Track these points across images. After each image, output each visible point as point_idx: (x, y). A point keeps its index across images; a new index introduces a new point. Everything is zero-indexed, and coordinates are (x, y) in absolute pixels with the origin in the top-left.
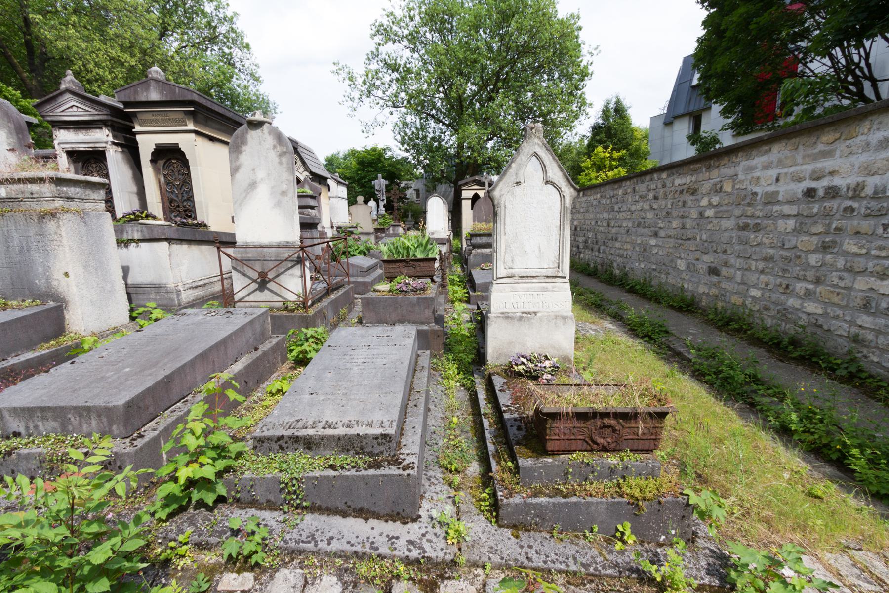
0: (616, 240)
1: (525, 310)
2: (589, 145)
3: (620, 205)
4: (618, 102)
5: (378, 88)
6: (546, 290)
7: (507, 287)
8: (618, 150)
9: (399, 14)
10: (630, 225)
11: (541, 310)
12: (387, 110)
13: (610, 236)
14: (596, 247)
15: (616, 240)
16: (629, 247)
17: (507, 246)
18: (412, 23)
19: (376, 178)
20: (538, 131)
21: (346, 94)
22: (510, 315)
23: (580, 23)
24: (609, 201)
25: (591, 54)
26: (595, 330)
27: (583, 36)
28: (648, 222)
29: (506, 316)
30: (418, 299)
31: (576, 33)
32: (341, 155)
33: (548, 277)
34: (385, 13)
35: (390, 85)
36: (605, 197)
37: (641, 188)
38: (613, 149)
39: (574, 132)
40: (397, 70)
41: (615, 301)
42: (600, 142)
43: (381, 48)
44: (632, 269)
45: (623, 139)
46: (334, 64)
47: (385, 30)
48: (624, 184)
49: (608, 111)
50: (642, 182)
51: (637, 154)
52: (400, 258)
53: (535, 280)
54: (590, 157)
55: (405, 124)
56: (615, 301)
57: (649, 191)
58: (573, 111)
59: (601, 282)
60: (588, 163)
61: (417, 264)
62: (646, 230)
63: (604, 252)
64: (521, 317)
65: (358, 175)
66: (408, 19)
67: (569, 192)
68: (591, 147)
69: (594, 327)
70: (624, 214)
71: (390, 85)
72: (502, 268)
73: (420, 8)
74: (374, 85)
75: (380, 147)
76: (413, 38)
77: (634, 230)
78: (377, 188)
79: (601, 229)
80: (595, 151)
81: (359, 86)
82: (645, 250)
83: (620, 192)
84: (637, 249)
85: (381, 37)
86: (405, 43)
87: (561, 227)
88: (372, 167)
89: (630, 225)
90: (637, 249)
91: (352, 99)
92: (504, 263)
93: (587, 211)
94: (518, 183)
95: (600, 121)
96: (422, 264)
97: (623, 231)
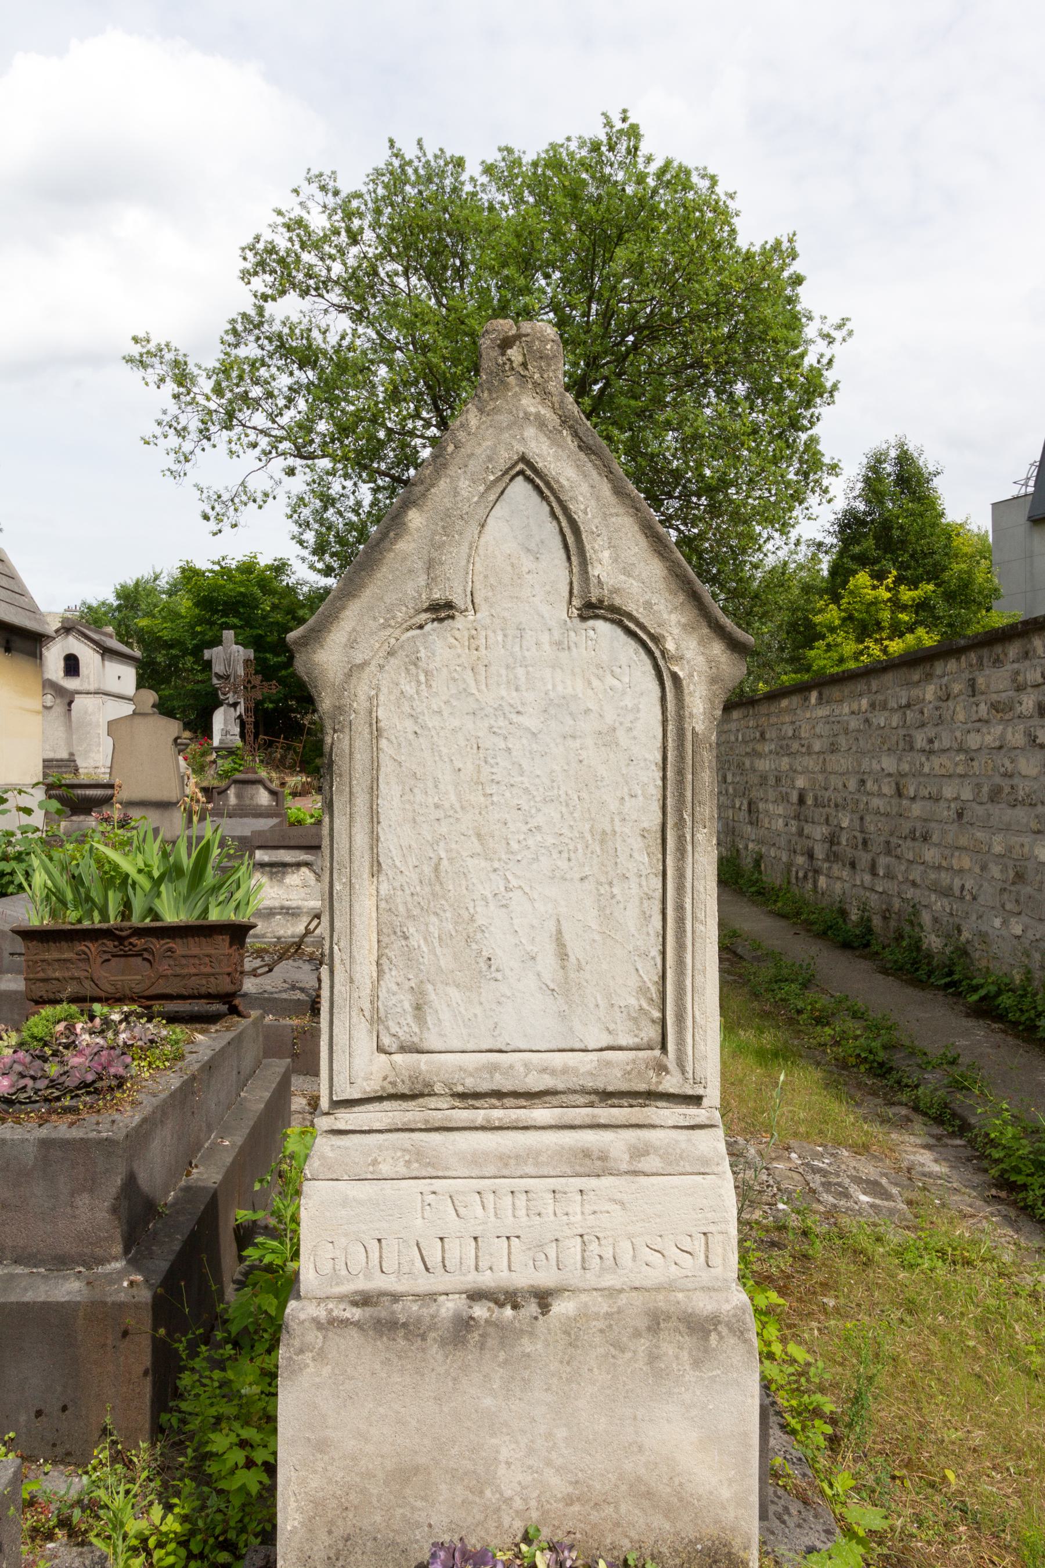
0: (926, 838)
1: (486, 1280)
2: (834, 570)
3: (930, 731)
4: (901, 446)
5: (254, 404)
6: (595, 1164)
7: (389, 1153)
8: (914, 584)
9: (318, 222)
10: (967, 794)
11: (573, 1276)
12: (278, 464)
13: (906, 827)
14: (864, 859)
15: (926, 838)
16: (966, 862)
17: (389, 932)
18: (354, 250)
19: (217, 642)
20: (535, 355)
21: (167, 418)
22: (404, 1311)
23: (796, 267)
24: (895, 720)
25: (829, 338)
26: (873, 1187)
27: (807, 298)
28: (1023, 789)
29: (383, 1319)
30: (45, 1144)
31: (788, 292)
32: (163, 583)
33: (606, 1096)
34: (280, 220)
35: (290, 400)
36: (884, 707)
37: (996, 680)
38: (899, 580)
39: (794, 534)
40: (314, 366)
41: (935, 1051)
42: (863, 560)
43: (270, 307)
44: (983, 936)
45: (925, 555)
46: (136, 340)
47: (282, 261)
48: (939, 668)
49: (879, 480)
50: (997, 662)
51: (963, 594)
52: (95, 921)
53: (541, 1114)
54: (836, 599)
55: (328, 501)
56: (935, 1051)
57: (1020, 689)
58: (788, 484)
59: (885, 971)
60: (833, 615)
61: (158, 945)
62: (1021, 814)
63: (890, 876)
64: (464, 1325)
65: (194, 635)
66: (344, 238)
67: (702, 664)
68: (840, 573)
69: (868, 1170)
70: (944, 759)
71: (290, 400)
72: (364, 1043)
73: (378, 212)
74: (245, 397)
75: (265, 560)
76: (359, 287)
77: (980, 810)
78: (218, 668)
79: (876, 802)
80: (851, 585)
81: (200, 399)
82: (1020, 877)
83: (930, 692)
84: (995, 871)
85: (269, 278)
86: (335, 296)
87: (669, 838)
88: (237, 614)
89: (967, 794)
90: (995, 871)
91: (182, 433)
92: (377, 1020)
93: (833, 749)
94: (442, 610)
95: (862, 507)
96: (179, 947)
97: (946, 813)
